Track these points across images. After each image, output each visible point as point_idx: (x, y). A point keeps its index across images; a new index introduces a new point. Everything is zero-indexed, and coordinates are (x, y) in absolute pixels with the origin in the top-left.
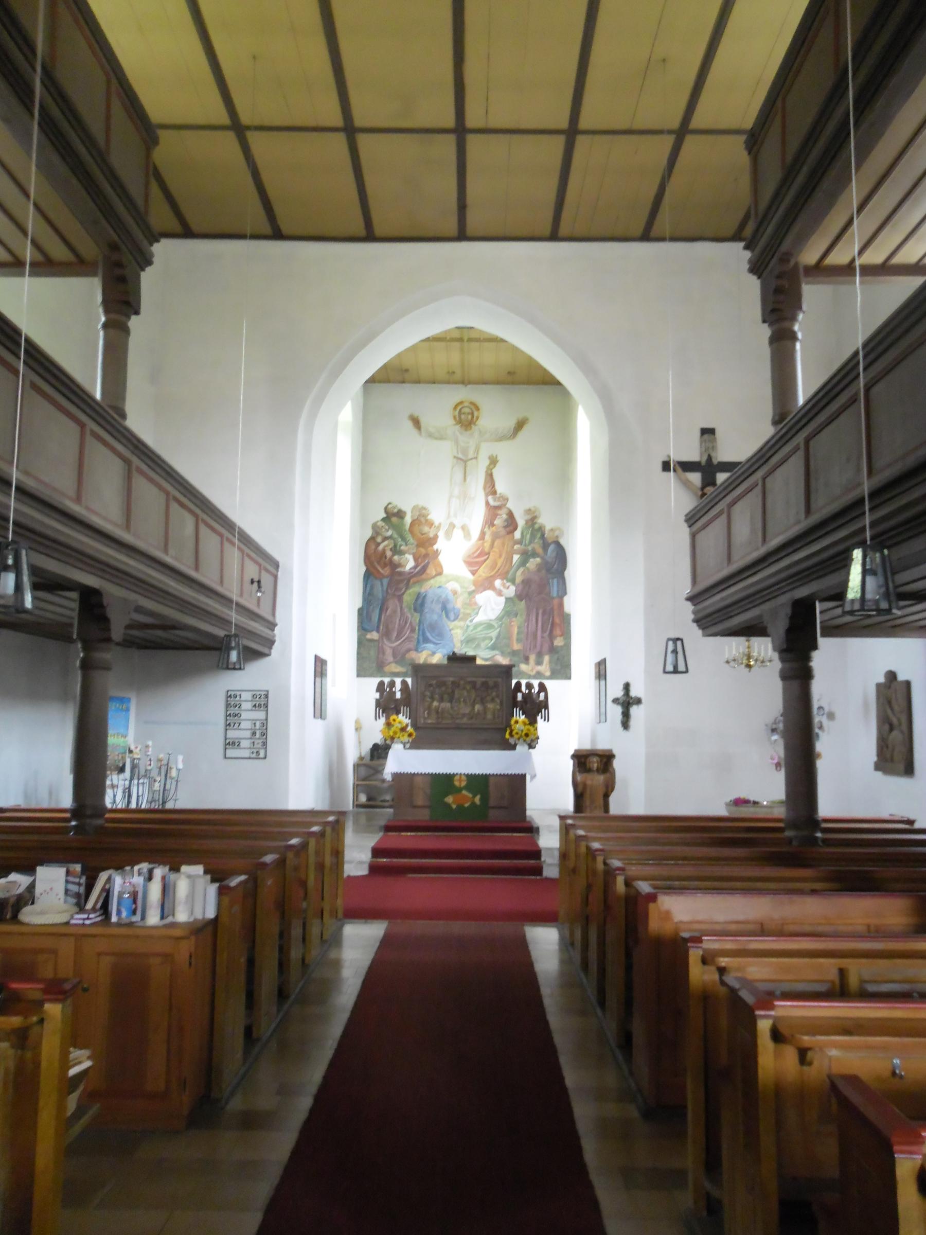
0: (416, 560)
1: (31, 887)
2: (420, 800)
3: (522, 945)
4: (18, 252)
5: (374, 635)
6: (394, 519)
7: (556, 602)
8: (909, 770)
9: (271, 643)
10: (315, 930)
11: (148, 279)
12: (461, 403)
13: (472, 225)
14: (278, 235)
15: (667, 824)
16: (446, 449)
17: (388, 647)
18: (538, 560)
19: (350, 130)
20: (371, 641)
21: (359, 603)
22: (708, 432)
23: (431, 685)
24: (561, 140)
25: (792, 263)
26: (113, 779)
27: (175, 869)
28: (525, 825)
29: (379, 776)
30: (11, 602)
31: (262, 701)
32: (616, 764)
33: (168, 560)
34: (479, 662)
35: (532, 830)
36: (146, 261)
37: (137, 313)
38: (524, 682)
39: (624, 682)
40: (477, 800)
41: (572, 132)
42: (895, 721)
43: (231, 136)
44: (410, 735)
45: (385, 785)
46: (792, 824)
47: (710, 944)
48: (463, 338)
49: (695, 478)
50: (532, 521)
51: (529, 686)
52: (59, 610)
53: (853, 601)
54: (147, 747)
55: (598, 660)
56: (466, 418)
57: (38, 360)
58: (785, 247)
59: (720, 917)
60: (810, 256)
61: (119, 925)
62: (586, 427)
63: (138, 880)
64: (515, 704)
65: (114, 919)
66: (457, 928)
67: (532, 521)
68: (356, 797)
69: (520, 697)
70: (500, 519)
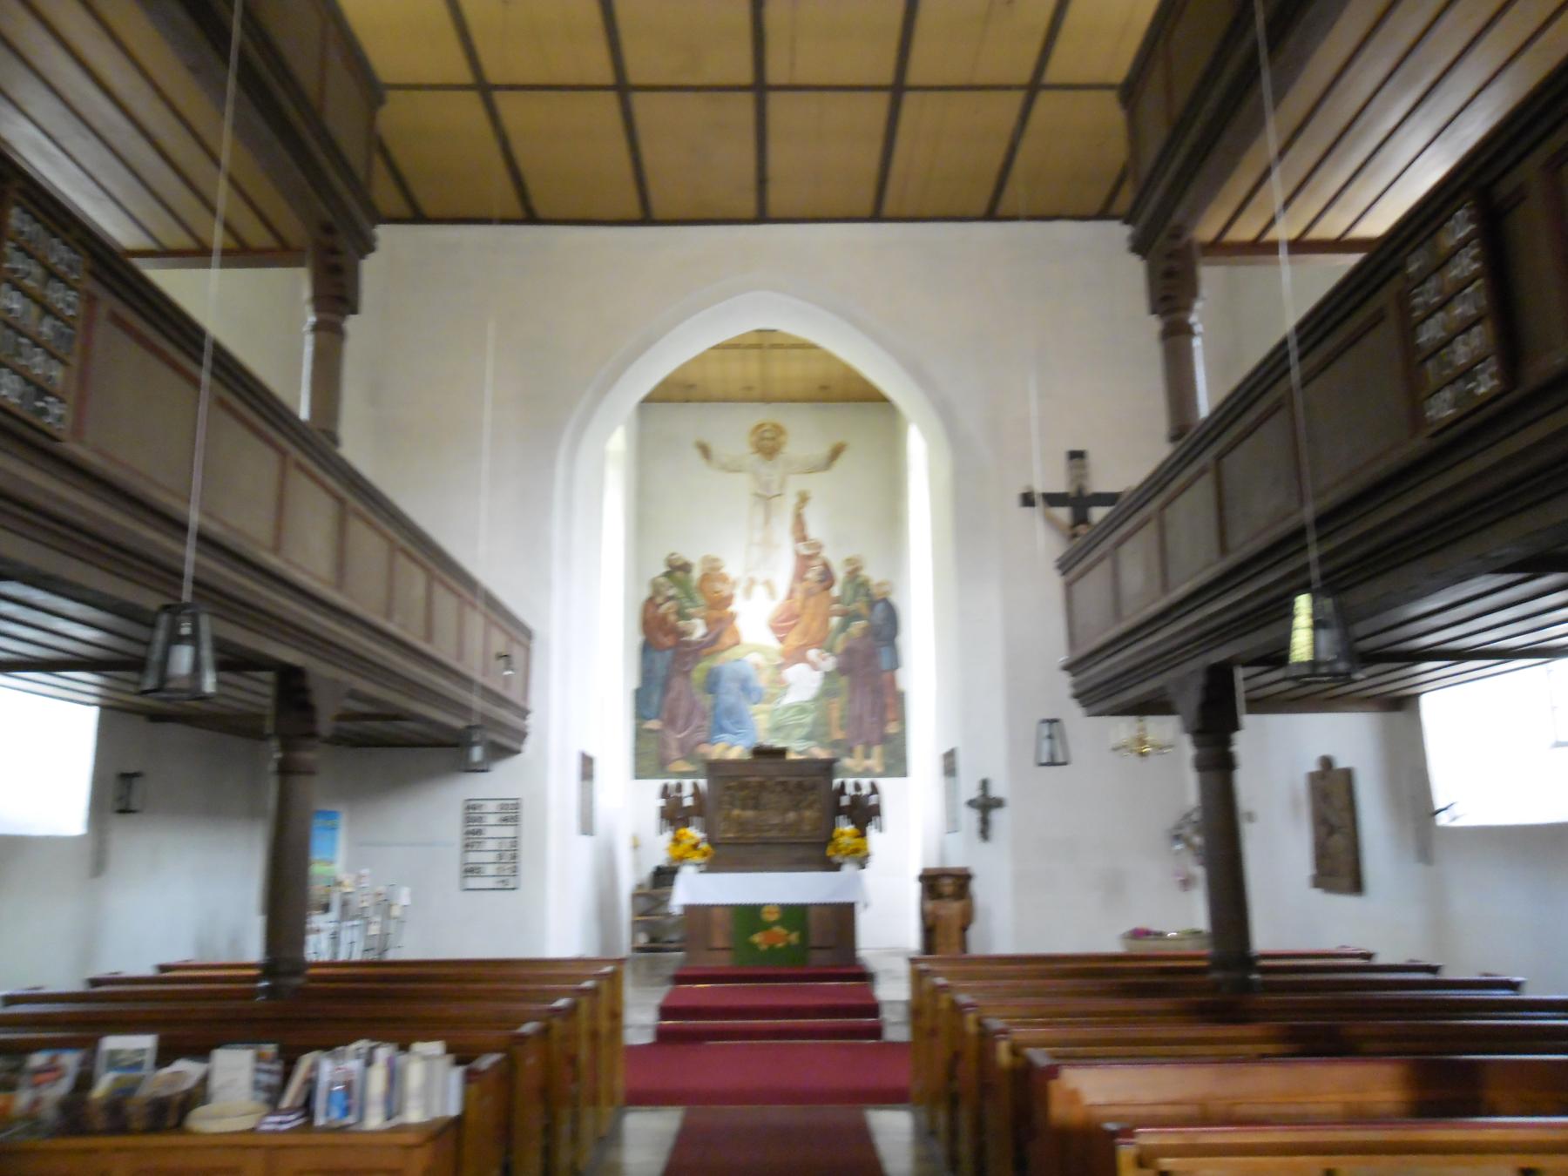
0: (708, 624)
1: (204, 1080)
2: (719, 941)
3: (864, 1137)
4: (201, 233)
5: (653, 724)
6: (679, 574)
7: (886, 676)
8: (1356, 885)
9: (521, 735)
10: (587, 1124)
11: (371, 270)
12: (761, 426)
13: (777, 199)
14: (530, 217)
15: (1329, 996)
16: (742, 485)
17: (674, 738)
18: (861, 624)
19: (622, 88)
20: (651, 731)
21: (634, 683)
22: (1076, 456)
23: (729, 788)
24: (883, 99)
25: (1184, 240)
26: (318, 921)
27: (404, 1047)
28: (855, 971)
29: (662, 910)
30: (185, 685)
31: (511, 813)
32: (977, 888)
33: (392, 627)
34: (792, 756)
35: (864, 977)
36: (367, 246)
37: (354, 311)
38: (850, 782)
39: (980, 777)
40: (794, 938)
41: (898, 89)
42: (1334, 820)
43: (473, 96)
44: (705, 854)
45: (670, 921)
46: (1219, 963)
47: (1148, 1138)
48: (764, 343)
49: (1063, 514)
50: (854, 574)
51: (857, 787)
52: (250, 697)
53: (1300, 664)
54: (360, 877)
55: (946, 749)
56: (768, 445)
57: (230, 371)
58: (1178, 216)
59: (1147, 1096)
60: (1206, 230)
61: (326, 1130)
62: (920, 450)
63: (354, 1065)
64: (840, 811)
65: (320, 1121)
66: (778, 1114)
67: (854, 574)
68: (634, 939)
69: (845, 801)
70: (815, 574)
